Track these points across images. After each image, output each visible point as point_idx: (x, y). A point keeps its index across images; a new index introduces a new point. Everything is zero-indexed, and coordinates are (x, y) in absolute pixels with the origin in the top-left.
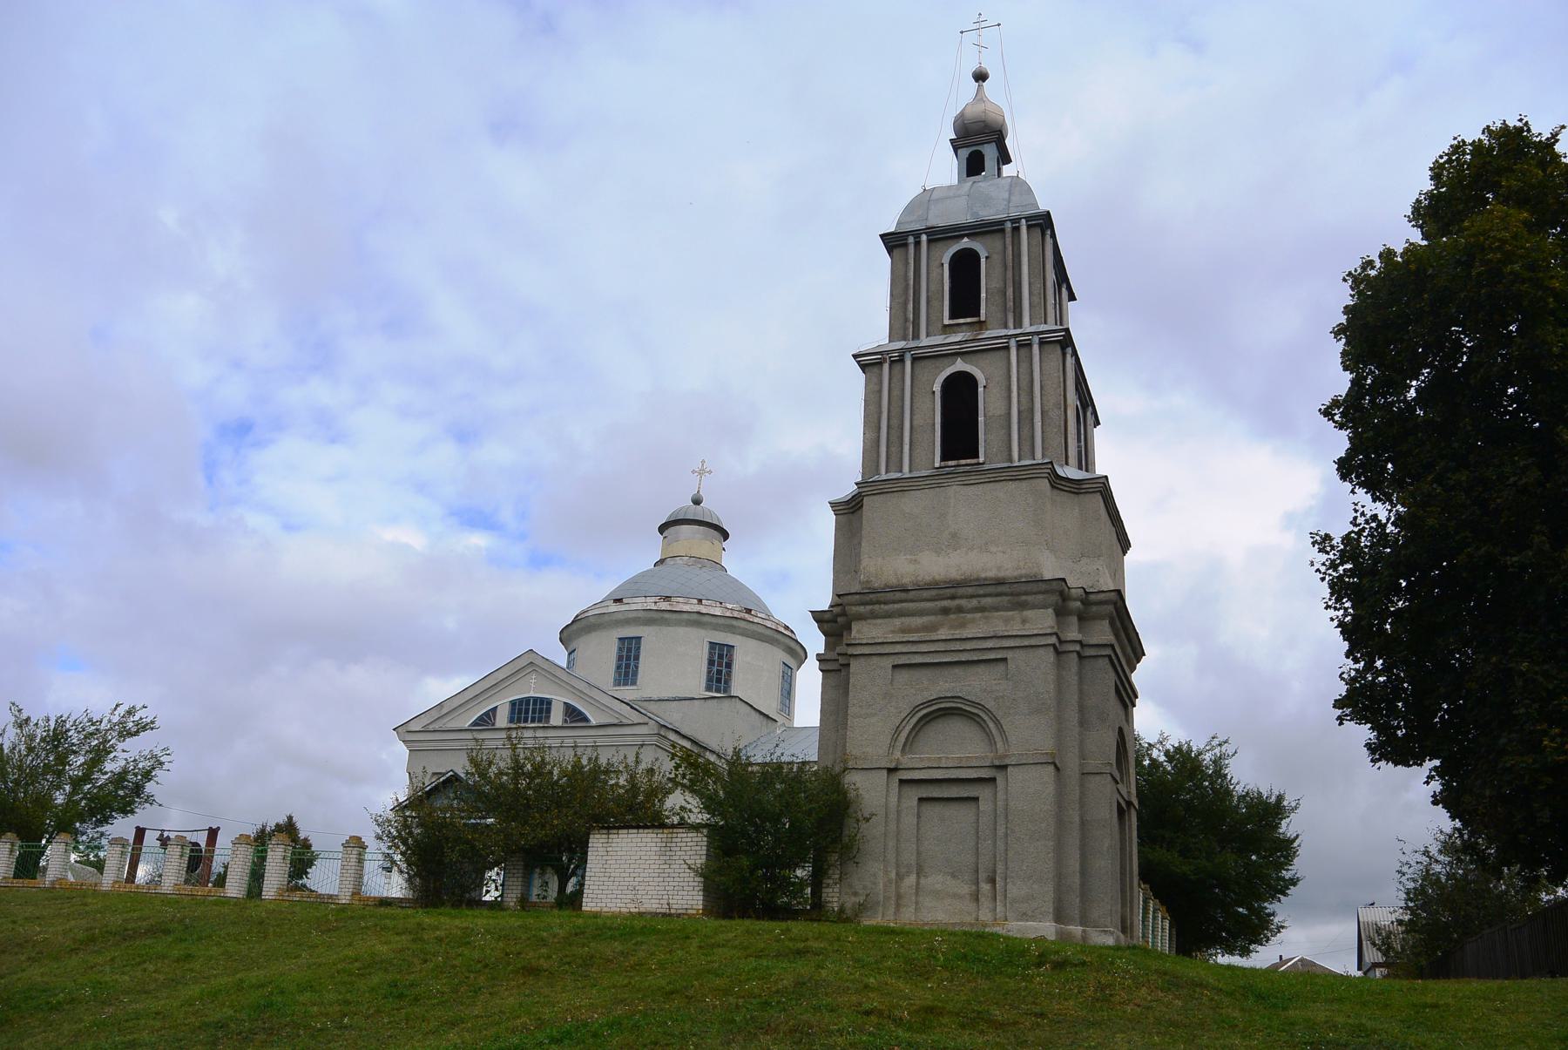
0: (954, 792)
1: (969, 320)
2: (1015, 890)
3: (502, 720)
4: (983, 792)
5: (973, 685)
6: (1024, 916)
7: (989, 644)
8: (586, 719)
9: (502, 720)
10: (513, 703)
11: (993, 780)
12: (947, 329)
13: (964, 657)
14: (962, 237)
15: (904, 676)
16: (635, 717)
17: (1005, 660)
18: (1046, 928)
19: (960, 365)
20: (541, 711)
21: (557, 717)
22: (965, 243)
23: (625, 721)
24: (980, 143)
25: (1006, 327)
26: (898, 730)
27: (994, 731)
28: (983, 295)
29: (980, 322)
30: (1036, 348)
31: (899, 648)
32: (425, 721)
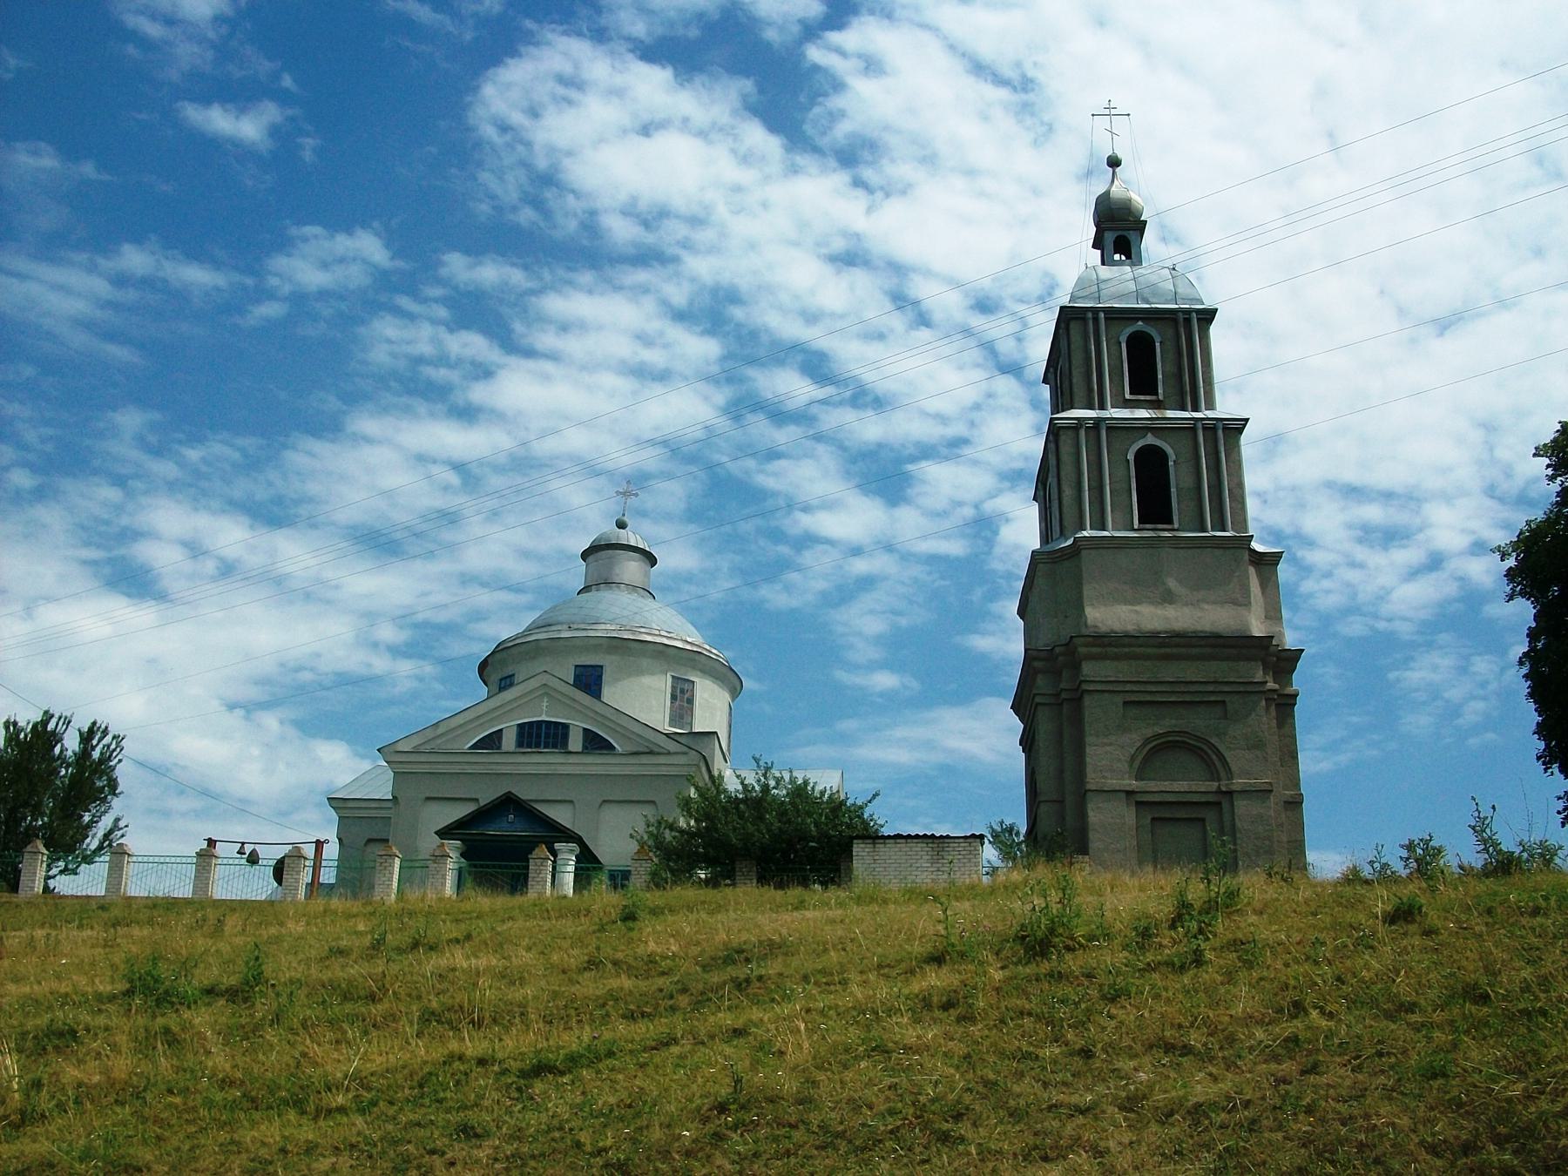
0: (1182, 814)
1: (1148, 398)
3: (509, 741)
4: (1210, 816)
5: (1198, 722)
7: (1211, 688)
9: (509, 741)
11: (1219, 804)
13: (1188, 698)
14: (1138, 319)
16: (672, 746)
18: (109, 988)
21: (575, 743)
23: (656, 750)
24: (1118, 229)
25: (1184, 409)
26: (1133, 758)
29: (1159, 401)
30: (1220, 433)
32: (415, 741)
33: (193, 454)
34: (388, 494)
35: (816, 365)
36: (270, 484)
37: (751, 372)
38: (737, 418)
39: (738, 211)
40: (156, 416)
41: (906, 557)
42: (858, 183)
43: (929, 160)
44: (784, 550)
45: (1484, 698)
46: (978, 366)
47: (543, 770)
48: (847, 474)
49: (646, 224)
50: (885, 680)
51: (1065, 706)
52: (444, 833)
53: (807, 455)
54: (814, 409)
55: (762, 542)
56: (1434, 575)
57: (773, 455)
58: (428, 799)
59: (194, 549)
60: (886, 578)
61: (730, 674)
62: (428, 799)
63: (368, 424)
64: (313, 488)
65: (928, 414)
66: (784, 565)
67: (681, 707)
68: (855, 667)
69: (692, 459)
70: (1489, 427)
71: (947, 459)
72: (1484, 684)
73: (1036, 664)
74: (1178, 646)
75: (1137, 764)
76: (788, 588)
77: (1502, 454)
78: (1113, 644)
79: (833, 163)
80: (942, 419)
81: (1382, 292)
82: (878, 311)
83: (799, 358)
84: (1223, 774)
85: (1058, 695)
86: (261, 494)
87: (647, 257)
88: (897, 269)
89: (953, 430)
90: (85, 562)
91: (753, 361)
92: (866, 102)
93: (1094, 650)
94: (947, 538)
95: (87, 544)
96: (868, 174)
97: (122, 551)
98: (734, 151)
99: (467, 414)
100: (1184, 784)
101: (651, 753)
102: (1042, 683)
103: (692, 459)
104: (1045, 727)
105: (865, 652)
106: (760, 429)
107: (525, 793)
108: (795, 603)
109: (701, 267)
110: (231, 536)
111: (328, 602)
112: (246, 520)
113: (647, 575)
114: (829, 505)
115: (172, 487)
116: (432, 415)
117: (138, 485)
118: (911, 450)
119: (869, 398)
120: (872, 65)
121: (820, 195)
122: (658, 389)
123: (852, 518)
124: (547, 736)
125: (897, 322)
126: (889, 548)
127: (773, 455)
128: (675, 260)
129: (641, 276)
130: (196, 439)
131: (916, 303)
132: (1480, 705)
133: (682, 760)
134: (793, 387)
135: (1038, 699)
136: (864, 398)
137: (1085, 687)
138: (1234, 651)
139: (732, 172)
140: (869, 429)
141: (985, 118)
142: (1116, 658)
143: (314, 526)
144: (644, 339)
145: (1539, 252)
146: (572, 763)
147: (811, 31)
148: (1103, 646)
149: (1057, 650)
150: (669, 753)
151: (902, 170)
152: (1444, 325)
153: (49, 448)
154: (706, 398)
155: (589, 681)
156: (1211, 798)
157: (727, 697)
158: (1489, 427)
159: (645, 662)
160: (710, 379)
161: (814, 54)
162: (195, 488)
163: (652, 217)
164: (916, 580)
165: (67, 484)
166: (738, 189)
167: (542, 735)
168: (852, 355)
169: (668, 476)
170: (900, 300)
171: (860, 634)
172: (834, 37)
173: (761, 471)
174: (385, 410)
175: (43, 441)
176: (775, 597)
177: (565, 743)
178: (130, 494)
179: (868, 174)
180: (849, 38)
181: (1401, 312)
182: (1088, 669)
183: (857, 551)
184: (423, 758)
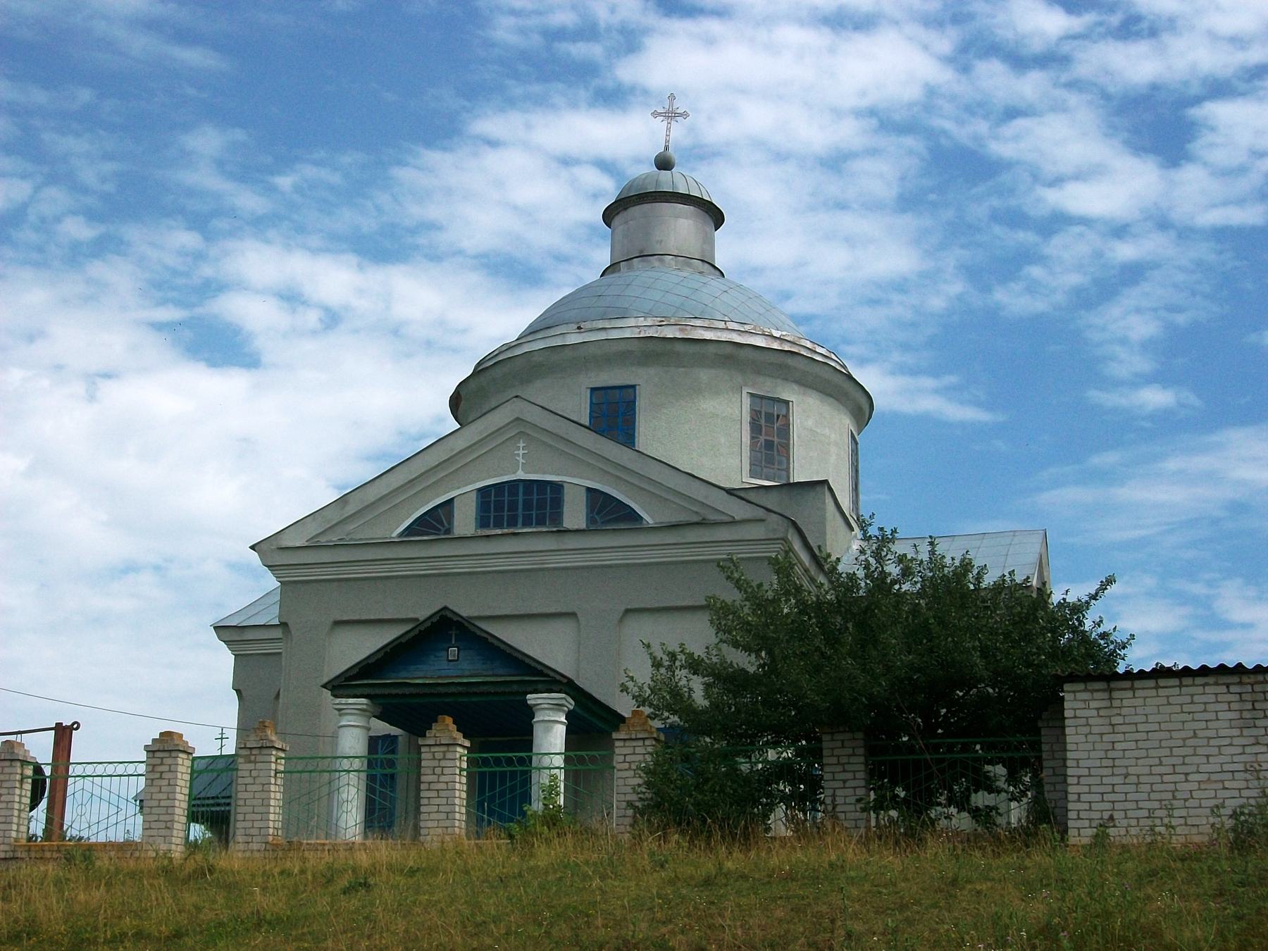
3: (465, 520)
6: (449, 814)
8: (633, 516)
9: (465, 520)
10: (483, 492)
16: (738, 510)
20: (541, 505)
21: (575, 514)
23: (713, 517)
32: (313, 529)
33: (285, 182)
34: (526, 213)
36: (379, 209)
38: (965, 69)
40: (239, 135)
41: (1186, 233)
44: (1026, 237)
47: (523, 564)
48: (1110, 130)
50: (1155, 398)
52: (341, 685)
53: (1059, 108)
54: (1066, 48)
55: (998, 230)
58: (338, 623)
59: (291, 297)
60: (1155, 265)
61: (848, 386)
62: (338, 623)
63: (490, 124)
64: (433, 212)
66: (1027, 256)
67: (769, 445)
68: (1118, 384)
69: (907, 128)
71: (1243, 94)
76: (1032, 288)
80: (1238, 41)
86: (368, 224)
90: (159, 327)
94: (1240, 202)
95: (163, 302)
97: (199, 311)
99: (614, 97)
101: (703, 523)
103: (907, 128)
105: (1133, 363)
106: (994, 78)
107: (465, 608)
110: (334, 279)
111: (455, 351)
112: (353, 259)
113: (710, 242)
114: (1081, 175)
115: (259, 225)
116: (574, 105)
117: (220, 224)
118: (1195, 89)
119: (1144, 25)
122: (861, 42)
124: (528, 505)
126: (1163, 224)
127: (1012, 113)
130: (284, 163)
133: (756, 532)
143: (435, 257)
146: (568, 549)
150: (733, 522)
153: (109, 187)
154: (926, 48)
155: (614, 415)
157: (846, 422)
159: (704, 375)
162: (280, 224)
164: (1199, 264)
165: (132, 233)
167: (519, 506)
169: (873, 152)
171: (1123, 341)
173: (996, 138)
174: (511, 103)
175: (104, 180)
176: (1013, 300)
177: (557, 517)
178: (209, 237)
183: (1120, 231)
184: (325, 556)
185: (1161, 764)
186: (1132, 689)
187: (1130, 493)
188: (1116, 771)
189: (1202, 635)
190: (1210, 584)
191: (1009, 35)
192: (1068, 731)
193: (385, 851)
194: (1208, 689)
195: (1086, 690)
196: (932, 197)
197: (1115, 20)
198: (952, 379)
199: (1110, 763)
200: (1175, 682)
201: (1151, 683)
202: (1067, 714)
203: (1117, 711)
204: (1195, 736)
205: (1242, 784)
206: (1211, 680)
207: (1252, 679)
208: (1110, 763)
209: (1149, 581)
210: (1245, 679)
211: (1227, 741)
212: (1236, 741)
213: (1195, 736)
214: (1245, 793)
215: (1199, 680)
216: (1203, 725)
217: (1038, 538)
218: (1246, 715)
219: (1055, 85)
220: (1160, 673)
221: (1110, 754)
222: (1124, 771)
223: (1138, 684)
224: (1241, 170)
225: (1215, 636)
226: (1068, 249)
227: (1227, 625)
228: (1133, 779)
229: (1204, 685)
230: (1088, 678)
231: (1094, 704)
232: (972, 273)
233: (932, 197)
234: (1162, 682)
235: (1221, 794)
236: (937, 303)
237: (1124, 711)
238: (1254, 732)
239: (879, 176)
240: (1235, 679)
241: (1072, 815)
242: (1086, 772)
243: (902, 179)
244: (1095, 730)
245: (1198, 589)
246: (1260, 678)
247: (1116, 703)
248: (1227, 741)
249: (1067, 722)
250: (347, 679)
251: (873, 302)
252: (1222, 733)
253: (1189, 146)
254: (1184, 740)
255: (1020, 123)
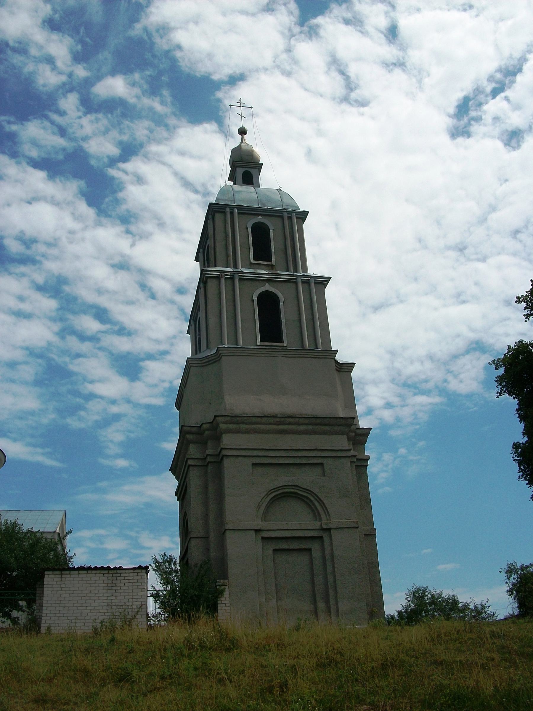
0: (295, 545)
1: (265, 263)
2: (344, 606)
4: (315, 546)
5: (306, 479)
11: (321, 538)
12: (251, 265)
13: (298, 461)
14: (259, 215)
15: (259, 470)
17: (322, 464)
19: (267, 287)
22: (260, 219)
27: (319, 507)
28: (273, 250)
31: (255, 453)
35: (101, 314)
37: (70, 316)
38: (63, 338)
39: (71, 242)
41: (136, 405)
42: (128, 232)
43: (161, 225)
45: (387, 471)
46: (176, 318)
49: (28, 247)
50: (122, 463)
51: (210, 467)
53: (95, 356)
54: (99, 335)
55: (69, 396)
56: (369, 417)
57: (78, 355)
60: (125, 415)
65: (152, 340)
68: (108, 457)
69: (40, 356)
70: (393, 353)
72: (387, 466)
73: (189, 437)
74: (289, 424)
75: (262, 508)
76: (80, 419)
77: (397, 365)
78: (242, 422)
79: (118, 222)
80: (158, 341)
81: (353, 293)
82: (134, 292)
83: (94, 310)
84: (323, 516)
85: (205, 459)
87: (25, 260)
88: (141, 271)
89: (163, 347)
91: (74, 313)
92: (134, 195)
93: (231, 426)
94: (155, 396)
96: (133, 228)
98: (73, 214)
100: (295, 520)
102: (193, 451)
103: (40, 356)
104: (195, 479)
106: (73, 342)
108: (83, 426)
109: (53, 266)
114: (101, 380)
118: (142, 356)
119: (126, 331)
120: (140, 180)
121: (109, 236)
122: (25, 323)
123: (113, 387)
125: (141, 296)
126: (128, 401)
127: (78, 355)
128: (40, 262)
129: (22, 269)
131: (150, 289)
132: (384, 475)
134: (91, 325)
135: (190, 462)
136: (123, 331)
137: (225, 452)
138: (328, 428)
139: (70, 223)
140: (123, 345)
141: (188, 207)
142: (247, 432)
144: (21, 299)
145: (416, 279)
147: (113, 162)
148: (238, 423)
149: (205, 426)
151: (149, 227)
152: (377, 308)
154: (49, 328)
156: (316, 534)
158: (393, 353)
160: (53, 320)
161: (113, 172)
163: (28, 242)
166: (72, 232)
168: (118, 311)
169: (26, 363)
170: (143, 286)
171: (112, 441)
172: (121, 165)
173: (72, 363)
176: (73, 423)
179: (133, 228)
180: (129, 166)
181: (360, 302)
182: (227, 440)
183: (113, 402)
185: (77, 603)
186: (70, 574)
187: (110, 497)
188: (61, 605)
189: (135, 551)
190: (138, 532)
191: (79, 328)
192: (45, 589)
193: (178, 633)
194: (97, 575)
195: (53, 574)
196: (46, 382)
197: (116, 328)
198: (48, 450)
199: (59, 602)
200: (85, 572)
201: (77, 572)
202: (45, 583)
203: (63, 582)
204: (91, 592)
205: (106, 611)
206: (98, 572)
207: (112, 572)
208: (59, 602)
209: (116, 531)
210: (110, 572)
211: (102, 595)
212: (105, 595)
213: (91, 592)
214: (107, 614)
215: (94, 572)
216: (94, 588)
217: (62, 514)
218: (109, 585)
219: (95, 348)
220: (81, 568)
221: (60, 599)
222: (64, 605)
223: (72, 572)
224: (156, 386)
225: (138, 552)
226: (94, 406)
227: (143, 548)
228: (67, 608)
229: (96, 573)
230: (54, 570)
231: (55, 580)
232: (59, 411)
233: (46, 382)
234: (81, 572)
235: (98, 614)
236: (45, 421)
237: (66, 582)
238: (111, 591)
239: (28, 372)
240: (107, 572)
241: (43, 622)
242: (50, 605)
243: (36, 374)
244: (55, 589)
245: (133, 534)
246: (115, 571)
247: (63, 579)
248: (102, 595)
249: (45, 586)
250: (186, 487)
251: (21, 418)
252: (100, 592)
253: (140, 375)
254: (87, 594)
255: (81, 359)
